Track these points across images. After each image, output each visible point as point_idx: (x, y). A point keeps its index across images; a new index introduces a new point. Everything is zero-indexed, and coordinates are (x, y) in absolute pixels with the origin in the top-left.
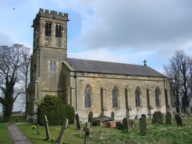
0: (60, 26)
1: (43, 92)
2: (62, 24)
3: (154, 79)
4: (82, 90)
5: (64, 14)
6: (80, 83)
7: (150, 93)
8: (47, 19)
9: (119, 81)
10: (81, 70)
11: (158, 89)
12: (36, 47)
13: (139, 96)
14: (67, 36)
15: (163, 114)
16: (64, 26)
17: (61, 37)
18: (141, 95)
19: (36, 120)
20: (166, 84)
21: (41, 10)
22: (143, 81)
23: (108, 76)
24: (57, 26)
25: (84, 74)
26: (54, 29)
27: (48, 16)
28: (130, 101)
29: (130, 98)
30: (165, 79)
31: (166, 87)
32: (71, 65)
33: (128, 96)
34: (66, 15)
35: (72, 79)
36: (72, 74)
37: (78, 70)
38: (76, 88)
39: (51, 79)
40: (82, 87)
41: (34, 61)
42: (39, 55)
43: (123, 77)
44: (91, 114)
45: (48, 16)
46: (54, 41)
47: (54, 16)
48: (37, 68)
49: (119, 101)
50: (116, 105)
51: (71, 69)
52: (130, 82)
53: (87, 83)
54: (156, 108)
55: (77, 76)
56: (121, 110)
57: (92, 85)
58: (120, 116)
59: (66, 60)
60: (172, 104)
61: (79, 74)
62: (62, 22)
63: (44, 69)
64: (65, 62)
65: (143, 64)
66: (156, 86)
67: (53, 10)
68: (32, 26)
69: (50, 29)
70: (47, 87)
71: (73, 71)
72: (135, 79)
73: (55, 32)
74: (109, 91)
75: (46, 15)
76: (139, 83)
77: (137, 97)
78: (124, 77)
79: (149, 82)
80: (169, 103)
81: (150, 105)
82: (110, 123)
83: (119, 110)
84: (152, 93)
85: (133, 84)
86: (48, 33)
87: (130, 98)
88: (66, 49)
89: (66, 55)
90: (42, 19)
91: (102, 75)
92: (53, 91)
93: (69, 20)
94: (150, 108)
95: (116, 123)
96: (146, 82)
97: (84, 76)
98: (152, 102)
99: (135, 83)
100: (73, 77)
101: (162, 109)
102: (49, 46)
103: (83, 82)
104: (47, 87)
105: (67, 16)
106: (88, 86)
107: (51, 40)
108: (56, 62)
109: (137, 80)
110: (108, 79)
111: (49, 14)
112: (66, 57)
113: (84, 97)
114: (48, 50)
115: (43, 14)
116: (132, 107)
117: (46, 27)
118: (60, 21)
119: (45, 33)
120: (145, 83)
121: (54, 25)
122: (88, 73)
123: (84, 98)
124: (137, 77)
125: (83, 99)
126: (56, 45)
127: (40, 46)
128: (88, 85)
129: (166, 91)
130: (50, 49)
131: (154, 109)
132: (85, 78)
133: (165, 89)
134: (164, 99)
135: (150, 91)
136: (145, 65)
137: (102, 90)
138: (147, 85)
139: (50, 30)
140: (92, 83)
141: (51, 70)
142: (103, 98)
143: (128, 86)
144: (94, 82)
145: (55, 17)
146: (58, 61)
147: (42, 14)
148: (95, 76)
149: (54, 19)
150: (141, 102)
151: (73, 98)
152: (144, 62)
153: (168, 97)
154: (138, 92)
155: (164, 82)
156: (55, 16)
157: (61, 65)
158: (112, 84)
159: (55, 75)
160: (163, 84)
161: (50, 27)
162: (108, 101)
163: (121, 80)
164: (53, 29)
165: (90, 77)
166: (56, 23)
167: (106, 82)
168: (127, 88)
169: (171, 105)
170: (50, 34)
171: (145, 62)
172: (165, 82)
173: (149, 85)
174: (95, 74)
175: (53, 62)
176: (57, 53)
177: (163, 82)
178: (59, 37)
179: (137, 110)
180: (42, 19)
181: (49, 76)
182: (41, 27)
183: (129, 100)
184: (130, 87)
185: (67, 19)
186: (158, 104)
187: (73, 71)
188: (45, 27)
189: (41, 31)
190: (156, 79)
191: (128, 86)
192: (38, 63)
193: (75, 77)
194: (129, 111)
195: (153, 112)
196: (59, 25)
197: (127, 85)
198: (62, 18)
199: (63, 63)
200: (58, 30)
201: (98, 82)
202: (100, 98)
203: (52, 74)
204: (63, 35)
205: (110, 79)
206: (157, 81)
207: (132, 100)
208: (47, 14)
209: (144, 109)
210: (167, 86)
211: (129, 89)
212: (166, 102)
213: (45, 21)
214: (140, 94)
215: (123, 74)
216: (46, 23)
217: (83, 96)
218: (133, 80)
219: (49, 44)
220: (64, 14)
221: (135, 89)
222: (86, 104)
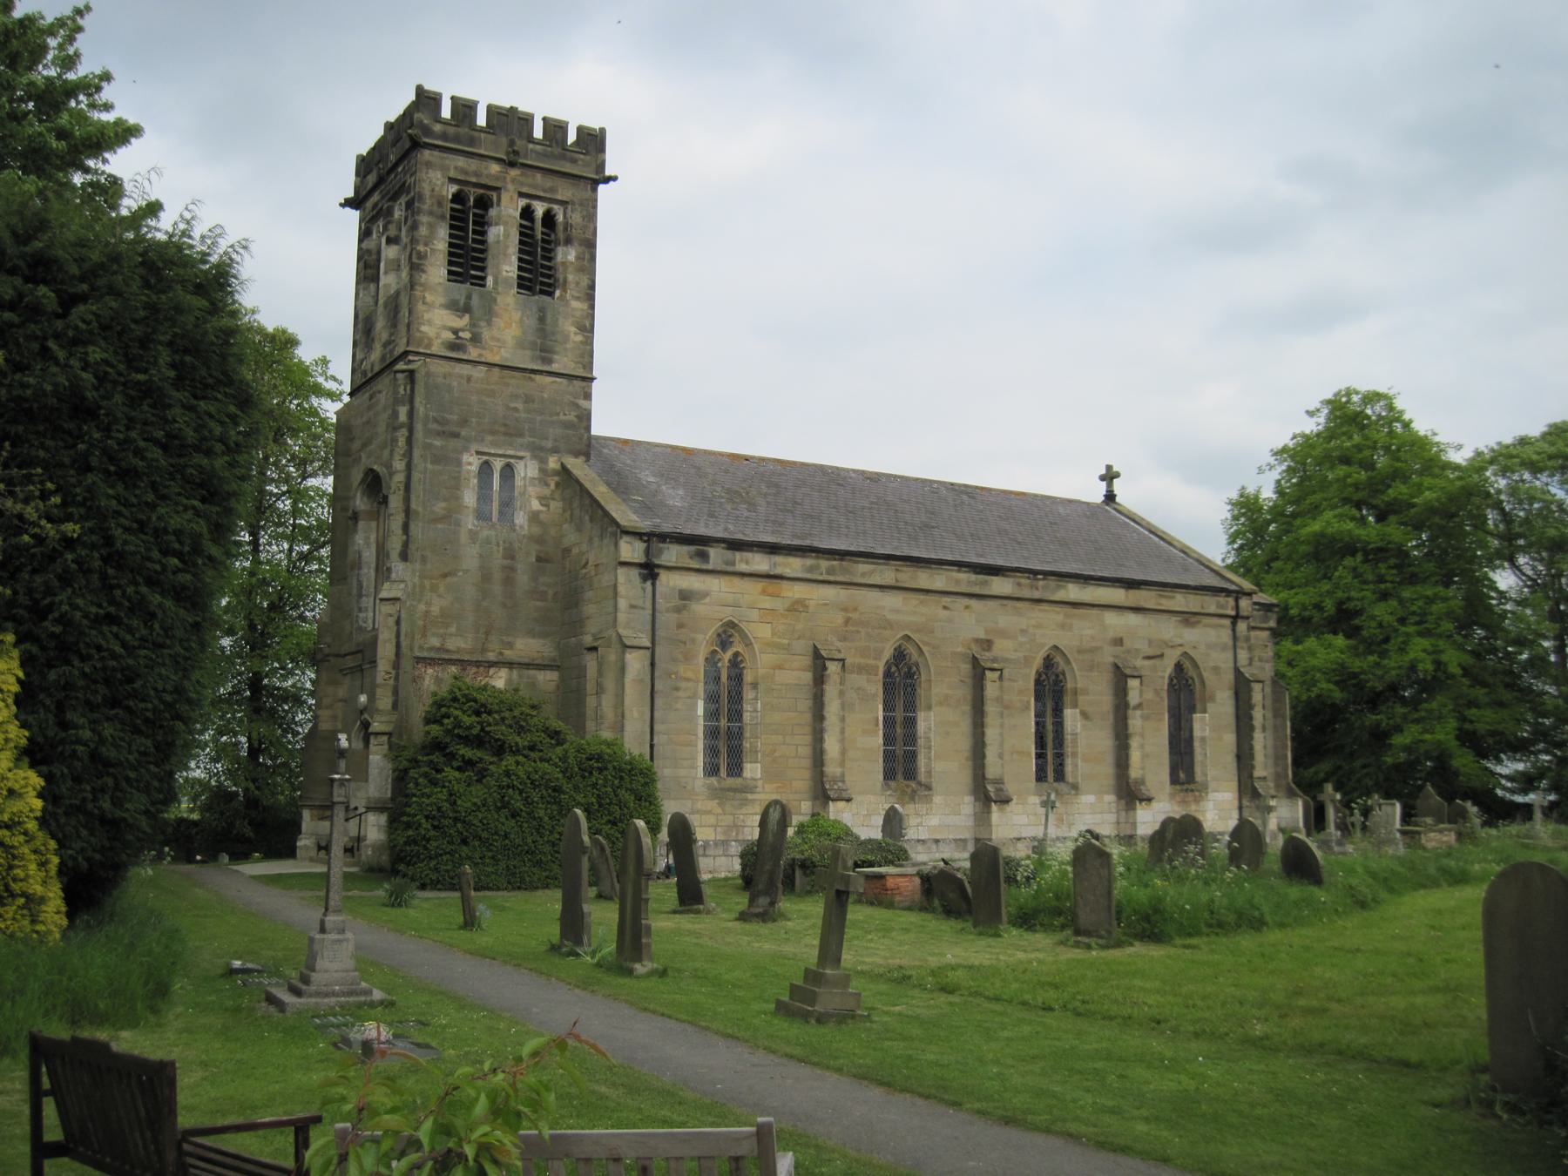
0: (549, 218)
1: (431, 662)
2: (563, 203)
3: (1166, 604)
4: (688, 658)
5: (492, 111)
6: (678, 610)
7: (1133, 697)
8: (461, 162)
9: (929, 610)
10: (687, 530)
11: (1192, 673)
12: (376, 355)
13: (1058, 712)
14: (592, 287)
15: (1214, 837)
16: (576, 218)
17: (551, 294)
18: (1075, 706)
19: (377, 848)
20: (1248, 639)
21: (426, 100)
22: (1095, 611)
23: (862, 569)
24: (527, 213)
25: (704, 556)
26: (507, 236)
27: (472, 141)
28: (1001, 745)
29: (1002, 726)
30: (1244, 603)
31: (1243, 655)
32: (621, 487)
33: (991, 709)
34: (593, 141)
35: (628, 583)
36: (631, 550)
37: (667, 528)
38: (653, 642)
39: (486, 577)
40: (693, 641)
41: (356, 445)
42: (411, 414)
43: (958, 582)
44: (775, 815)
45: (472, 141)
46: (509, 322)
47: (512, 143)
48: (395, 502)
49: (928, 739)
50: (901, 764)
51: (625, 515)
52: (1005, 618)
53: (727, 614)
54: (1172, 796)
55: (659, 566)
56: (937, 799)
57: (760, 631)
58: (939, 829)
59: (587, 456)
60: (1279, 777)
61: (672, 554)
62: (565, 192)
63: (440, 507)
64: (576, 466)
65: (1094, 493)
66: (1178, 652)
67: (506, 103)
68: (348, 203)
69: (483, 233)
70: (453, 630)
71: (639, 535)
72: (1037, 595)
73: (514, 259)
74: (861, 669)
75: (457, 139)
76: (1063, 626)
77: (1049, 721)
78: (965, 580)
79: (1133, 619)
80: (1262, 767)
81: (1134, 773)
82: (881, 877)
83: (928, 799)
84: (1149, 695)
85: (1023, 631)
86: (468, 262)
87: (1002, 726)
88: (584, 379)
89: (585, 417)
90: (429, 165)
91: (824, 564)
92: (491, 656)
93: (614, 179)
94: (1130, 794)
95: (920, 875)
96: (1111, 618)
97: (704, 567)
98: (1145, 756)
99: (1039, 626)
100: (634, 574)
101: (1210, 805)
102: (473, 353)
103: (698, 608)
104: (453, 630)
105: (601, 148)
106: (727, 634)
107: (490, 314)
108: (520, 468)
109: (1057, 608)
110: (864, 592)
111: (481, 130)
112: (588, 428)
113: (701, 704)
114: (469, 379)
115: (438, 128)
116: (1010, 788)
117: (457, 221)
118: (549, 182)
119: (450, 263)
120: (1093, 632)
121: (508, 209)
122: (736, 545)
123: (700, 711)
124: (1052, 582)
125: (695, 717)
126: (520, 344)
127: (418, 353)
128: (732, 625)
129: (1242, 688)
130: (479, 372)
131: (1154, 804)
132: (714, 584)
133: (1237, 671)
134: (1230, 738)
135: (1133, 684)
136: (1110, 497)
137: (819, 663)
138: (1119, 642)
139: (483, 242)
140: (755, 614)
141: (482, 515)
142: (1131, 730)
143: (987, 644)
144: (767, 614)
145: (516, 153)
146: (534, 457)
147: (427, 131)
148: (779, 571)
149: (512, 164)
150: (1075, 755)
151: (636, 714)
152: (1102, 478)
153: (1252, 728)
154: (1051, 689)
155: (1234, 624)
156: (520, 144)
157: (547, 485)
158: (890, 625)
159: (510, 554)
160: (1225, 636)
161: (482, 224)
162: (857, 738)
163: (946, 600)
164: (503, 234)
165: (743, 575)
166: (521, 195)
167: (845, 610)
168: (984, 656)
169: (1272, 785)
170: (483, 269)
171: (1110, 476)
172: (1242, 626)
173: (1127, 643)
174: (779, 559)
175: (498, 464)
176: (528, 400)
177: (1227, 622)
178: (542, 292)
179: (1044, 804)
180: (429, 165)
181: (470, 558)
182: (424, 219)
183: (991, 734)
184: (1002, 647)
185: (601, 166)
186: (1182, 765)
187: (639, 535)
188: (452, 218)
189: (421, 248)
190: (1180, 601)
191: (987, 644)
192: (399, 465)
193: (649, 571)
194: (994, 807)
195: (1148, 820)
196: (540, 209)
197: (982, 635)
198: (564, 157)
199: (565, 470)
200: (465, 229)
201: (798, 607)
202: (808, 717)
203: (487, 541)
204: (570, 277)
205: (875, 594)
206: (1189, 618)
207: (1013, 739)
208: (464, 130)
209: (1087, 799)
210: (1250, 649)
211: (995, 660)
212: (1239, 757)
213: (452, 180)
214: (1068, 699)
215: (960, 565)
216: (454, 188)
217: (694, 696)
218: (1027, 604)
219: (476, 339)
220: (492, 111)
221: (1038, 662)
222: (712, 752)
